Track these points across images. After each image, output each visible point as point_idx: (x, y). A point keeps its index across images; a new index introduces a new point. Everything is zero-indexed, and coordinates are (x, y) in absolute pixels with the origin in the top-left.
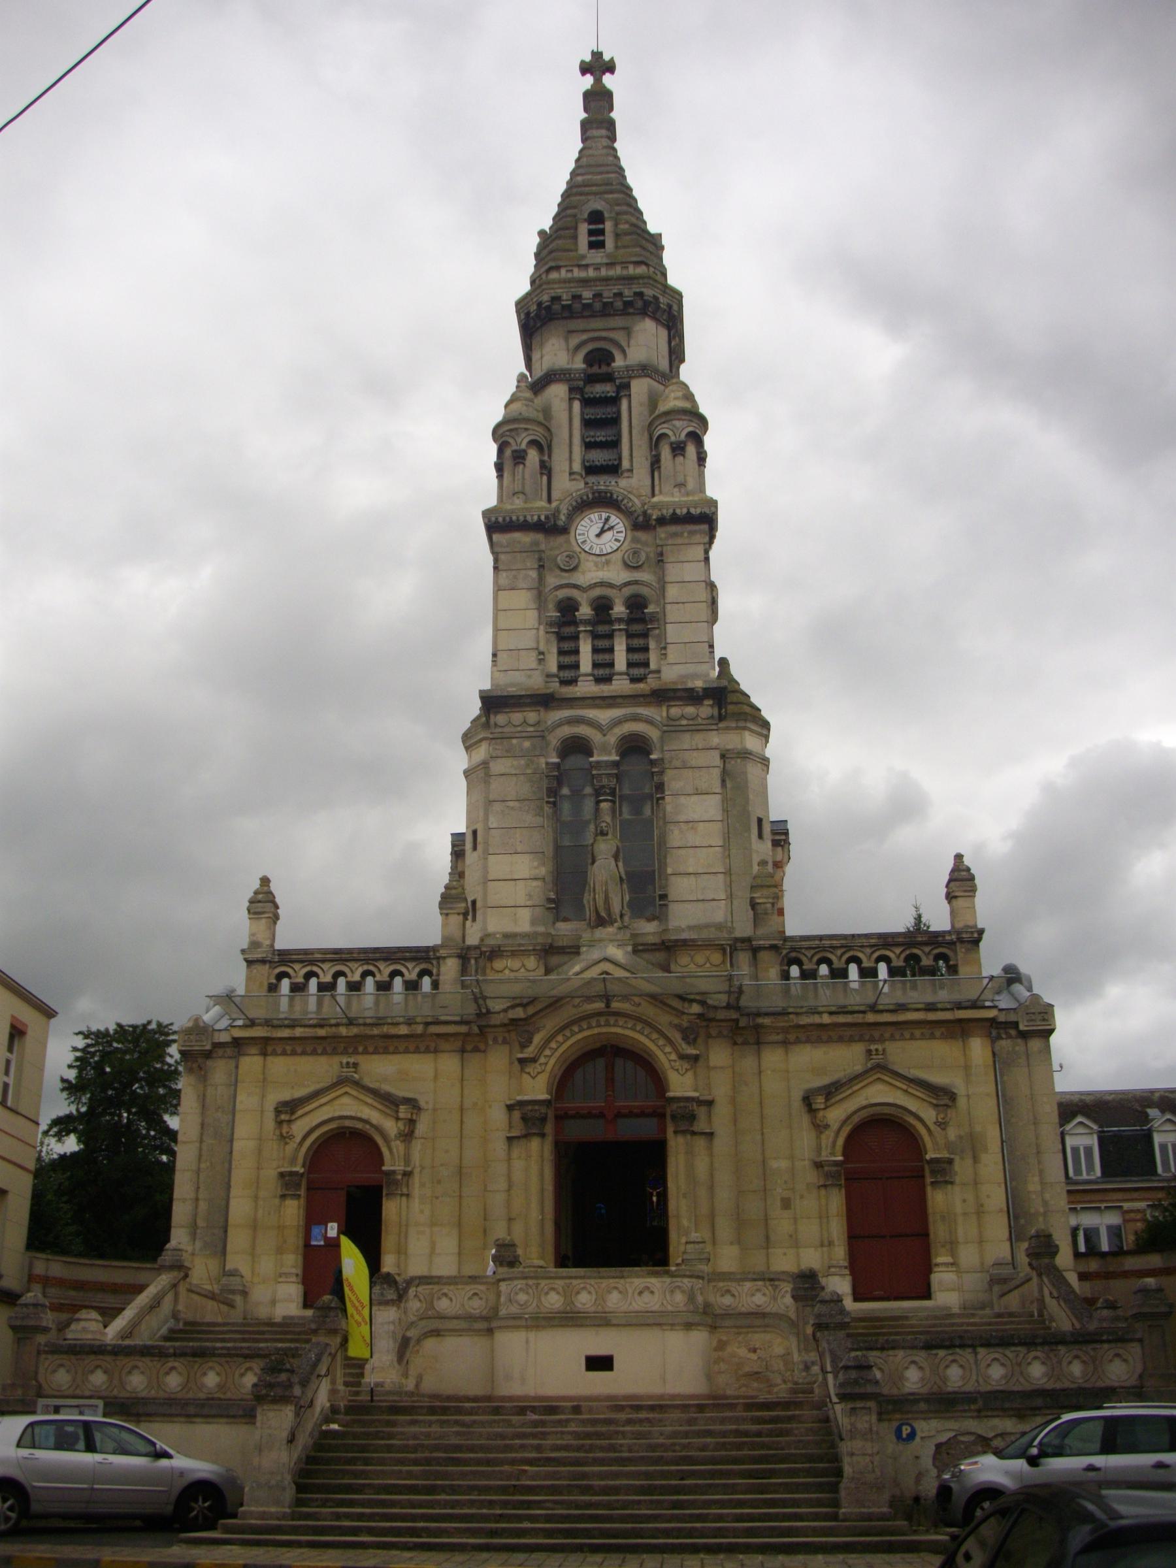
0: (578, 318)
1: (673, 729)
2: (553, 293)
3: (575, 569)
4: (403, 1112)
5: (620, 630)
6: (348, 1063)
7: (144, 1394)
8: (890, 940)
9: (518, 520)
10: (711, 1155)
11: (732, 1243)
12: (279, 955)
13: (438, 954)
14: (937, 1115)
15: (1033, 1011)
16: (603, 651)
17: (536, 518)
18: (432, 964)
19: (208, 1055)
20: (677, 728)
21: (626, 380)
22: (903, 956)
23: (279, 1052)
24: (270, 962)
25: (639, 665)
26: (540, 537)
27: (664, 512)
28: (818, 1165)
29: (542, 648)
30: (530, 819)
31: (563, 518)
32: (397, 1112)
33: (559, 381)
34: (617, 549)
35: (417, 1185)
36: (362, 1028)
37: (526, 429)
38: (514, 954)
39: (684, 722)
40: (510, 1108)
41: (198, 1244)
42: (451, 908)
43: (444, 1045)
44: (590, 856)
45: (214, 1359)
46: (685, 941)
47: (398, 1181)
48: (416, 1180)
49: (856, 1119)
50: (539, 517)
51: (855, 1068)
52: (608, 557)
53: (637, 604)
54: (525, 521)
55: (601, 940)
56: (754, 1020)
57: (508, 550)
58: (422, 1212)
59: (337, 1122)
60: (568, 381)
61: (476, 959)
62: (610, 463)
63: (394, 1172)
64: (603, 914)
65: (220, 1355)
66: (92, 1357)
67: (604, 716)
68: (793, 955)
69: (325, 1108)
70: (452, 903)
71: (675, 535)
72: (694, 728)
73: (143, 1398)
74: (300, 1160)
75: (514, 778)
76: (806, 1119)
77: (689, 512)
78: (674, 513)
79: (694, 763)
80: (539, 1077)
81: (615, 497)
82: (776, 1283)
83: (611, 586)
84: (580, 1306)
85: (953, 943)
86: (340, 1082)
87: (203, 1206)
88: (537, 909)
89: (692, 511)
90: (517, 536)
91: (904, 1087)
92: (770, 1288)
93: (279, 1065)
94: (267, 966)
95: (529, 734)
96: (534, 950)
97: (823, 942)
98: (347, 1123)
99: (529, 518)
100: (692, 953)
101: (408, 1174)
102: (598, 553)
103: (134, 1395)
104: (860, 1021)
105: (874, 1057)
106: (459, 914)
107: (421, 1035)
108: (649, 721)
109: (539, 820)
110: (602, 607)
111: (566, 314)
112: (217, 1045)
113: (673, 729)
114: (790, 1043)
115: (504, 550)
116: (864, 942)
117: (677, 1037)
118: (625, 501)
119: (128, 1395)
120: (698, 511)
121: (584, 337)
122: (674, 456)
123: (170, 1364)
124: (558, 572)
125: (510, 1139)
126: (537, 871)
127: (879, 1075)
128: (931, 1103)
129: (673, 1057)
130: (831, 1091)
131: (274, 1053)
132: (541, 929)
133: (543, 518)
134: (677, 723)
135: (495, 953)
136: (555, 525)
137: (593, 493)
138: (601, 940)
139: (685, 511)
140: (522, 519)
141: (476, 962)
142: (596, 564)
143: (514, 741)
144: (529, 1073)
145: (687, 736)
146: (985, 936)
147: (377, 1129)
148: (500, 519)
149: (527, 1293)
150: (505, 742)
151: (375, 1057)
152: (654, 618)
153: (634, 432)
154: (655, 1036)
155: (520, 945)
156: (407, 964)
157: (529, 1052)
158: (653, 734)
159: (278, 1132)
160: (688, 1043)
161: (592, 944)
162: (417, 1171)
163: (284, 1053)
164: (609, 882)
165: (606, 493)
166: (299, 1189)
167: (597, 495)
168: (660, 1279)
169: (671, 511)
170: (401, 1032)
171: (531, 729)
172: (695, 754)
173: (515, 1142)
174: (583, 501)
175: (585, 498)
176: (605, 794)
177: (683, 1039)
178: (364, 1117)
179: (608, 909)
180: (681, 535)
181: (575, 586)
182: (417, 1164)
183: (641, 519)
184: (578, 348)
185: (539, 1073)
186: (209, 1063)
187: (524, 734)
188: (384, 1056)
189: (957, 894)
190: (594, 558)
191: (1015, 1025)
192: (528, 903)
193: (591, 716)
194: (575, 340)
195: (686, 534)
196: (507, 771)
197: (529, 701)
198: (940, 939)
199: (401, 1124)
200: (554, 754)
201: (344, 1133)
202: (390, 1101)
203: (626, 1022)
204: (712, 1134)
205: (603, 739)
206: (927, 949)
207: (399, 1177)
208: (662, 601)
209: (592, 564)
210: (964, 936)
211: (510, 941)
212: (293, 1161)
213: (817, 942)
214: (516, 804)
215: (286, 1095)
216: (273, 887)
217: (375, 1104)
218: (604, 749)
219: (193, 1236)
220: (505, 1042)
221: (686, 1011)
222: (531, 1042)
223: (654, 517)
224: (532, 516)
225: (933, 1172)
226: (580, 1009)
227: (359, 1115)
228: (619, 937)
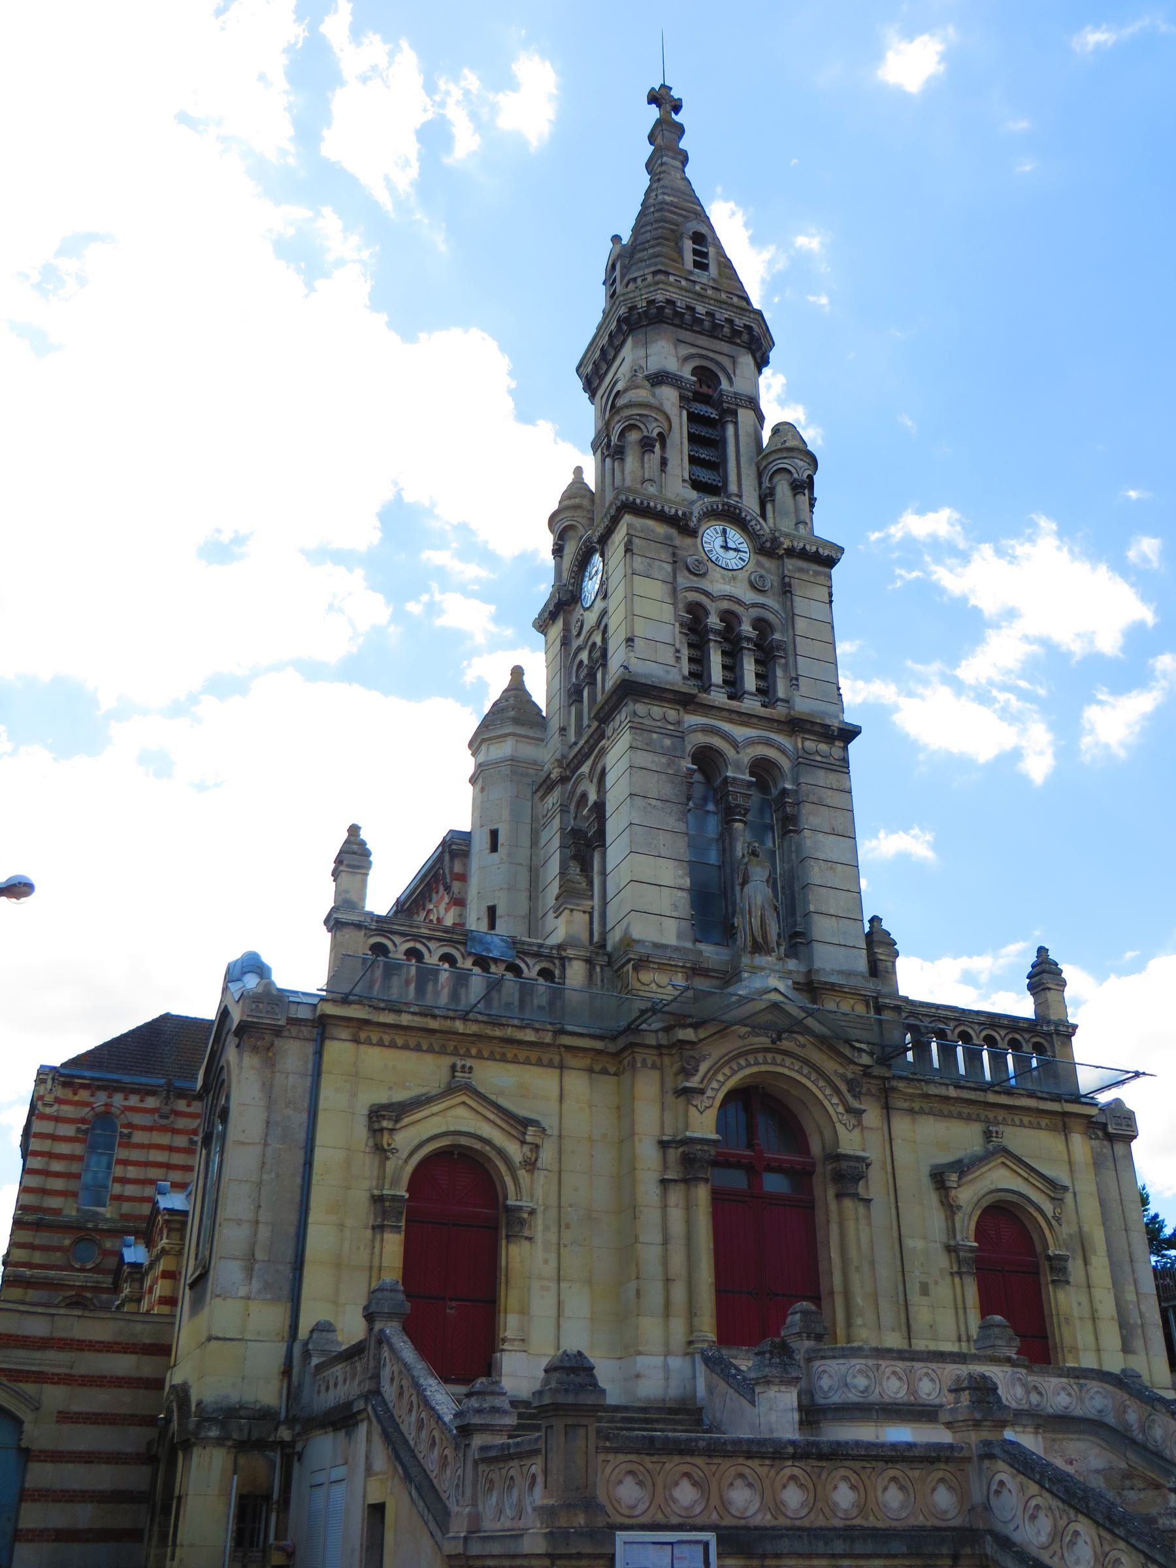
0: (686, 329)
1: (808, 762)
2: (668, 295)
3: (703, 575)
4: (531, 1134)
5: (749, 649)
6: (463, 1067)
7: (757, 1521)
8: (996, 1020)
9: (655, 508)
10: (870, 1224)
11: (893, 1330)
12: (377, 922)
13: (564, 954)
14: (1054, 1209)
15: (1118, 1115)
16: (732, 668)
17: (673, 511)
18: (554, 964)
19: (278, 1032)
20: (812, 763)
21: (733, 407)
22: (1007, 1039)
23: (374, 1042)
24: (366, 928)
25: (765, 692)
26: (673, 532)
27: (796, 544)
28: (950, 1249)
29: (678, 646)
30: (672, 822)
31: (694, 519)
32: (524, 1134)
33: (672, 385)
34: (742, 568)
35: (540, 1228)
36: (482, 1026)
37: (656, 420)
38: (662, 967)
39: (819, 758)
40: (663, 1145)
41: (256, 1284)
42: (578, 905)
43: (570, 1060)
44: (741, 876)
45: (847, 1463)
46: (833, 984)
47: (525, 1220)
48: (539, 1220)
49: (984, 1204)
50: (677, 511)
51: (975, 1148)
52: (734, 573)
53: (761, 625)
54: (662, 511)
55: (762, 969)
56: (889, 1082)
57: (642, 535)
58: (546, 1262)
59: (452, 1137)
60: (679, 388)
61: (602, 966)
62: (714, 483)
63: (520, 1208)
64: (760, 940)
65: (854, 1458)
66: (677, 1459)
67: (740, 732)
68: (912, 1021)
69: (435, 1119)
70: (579, 898)
71: (801, 570)
72: (824, 765)
73: (756, 1528)
74: (405, 1182)
75: (656, 775)
76: (933, 1198)
77: (817, 551)
78: (804, 548)
79: (829, 802)
80: (708, 1112)
81: (743, 515)
82: (1082, 1381)
83: (739, 602)
84: (925, 1396)
85: (1049, 1034)
86: (450, 1090)
87: (264, 1233)
88: (684, 922)
89: (821, 551)
90: (650, 523)
91: (1026, 1175)
92: (1075, 1387)
93: (374, 1058)
94: (363, 932)
95: (668, 732)
96: (682, 967)
97: (939, 1011)
98: (463, 1141)
99: (666, 509)
100: (838, 999)
101: (532, 1212)
102: (724, 566)
103: (742, 1522)
104: (981, 1099)
105: (994, 1139)
106: (584, 912)
107: (548, 1045)
108: (783, 751)
109: (681, 827)
110: (729, 618)
111: (676, 321)
112: (294, 1021)
113: (808, 762)
114: (916, 1112)
115: (637, 534)
116: (977, 1019)
117: (843, 1088)
118: (753, 523)
119: (788, 1523)
120: (826, 553)
121: (693, 351)
122: (795, 495)
123: (787, 1472)
124: (686, 573)
125: (664, 1183)
126: (681, 881)
127: (1003, 1159)
128: (1048, 1195)
129: (841, 1109)
130: (962, 1168)
131: (369, 1042)
132: (689, 945)
133: (680, 513)
134: (812, 758)
135: (642, 963)
136: (687, 525)
137: (723, 505)
138: (762, 969)
139: (814, 549)
140: (659, 507)
141: (602, 970)
142: (723, 577)
143: (655, 736)
144: (696, 1106)
145: (821, 773)
146: (1078, 1031)
147: (500, 1152)
148: (638, 501)
149: (868, 1377)
150: (645, 734)
151: (490, 1063)
152: (780, 646)
153: (743, 460)
154: (822, 1083)
155: (670, 959)
156: (528, 960)
157: (694, 1082)
158: (785, 764)
159: (371, 1143)
160: (855, 1096)
161: (755, 970)
162: (540, 1209)
163: (380, 1044)
164: (766, 906)
165: (735, 508)
166: (400, 1221)
167: (726, 507)
168: (1001, 1368)
169: (801, 545)
170: (527, 1038)
171: (672, 728)
172: (830, 792)
173: (672, 1186)
174: (713, 510)
175: (715, 507)
176: (739, 814)
177: (849, 1091)
178: (485, 1135)
179: (765, 936)
180: (807, 572)
181: (706, 593)
182: (540, 1201)
183: (768, 545)
184: (687, 359)
185: (707, 1108)
186: (278, 1042)
187: (664, 731)
188: (501, 1064)
189: (1050, 986)
190: (722, 570)
191: (1104, 1126)
192: (674, 914)
193: (726, 729)
194: (685, 351)
195: (811, 573)
196: (649, 766)
197: (671, 696)
198: (1039, 1028)
199: (526, 1148)
200: (689, 759)
201: (452, 1153)
202: (520, 1124)
203: (793, 1063)
204: (869, 1201)
205: (736, 756)
206: (1027, 1036)
207: (525, 1215)
208: (791, 631)
209: (719, 575)
210: (1061, 1029)
211: (659, 952)
212: (395, 1183)
213: (933, 1010)
214: (658, 803)
215: (382, 1097)
216: (364, 835)
217: (499, 1122)
218: (738, 767)
219: (249, 1271)
220: (654, 1067)
221: (856, 1060)
222: (697, 1071)
223: (785, 546)
224: (671, 508)
225: (1052, 1268)
226: (746, 1042)
227: (479, 1133)
228: (777, 968)
